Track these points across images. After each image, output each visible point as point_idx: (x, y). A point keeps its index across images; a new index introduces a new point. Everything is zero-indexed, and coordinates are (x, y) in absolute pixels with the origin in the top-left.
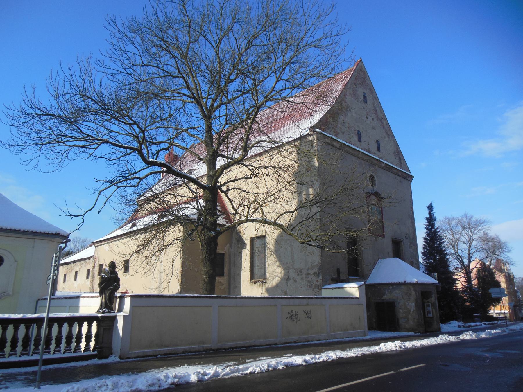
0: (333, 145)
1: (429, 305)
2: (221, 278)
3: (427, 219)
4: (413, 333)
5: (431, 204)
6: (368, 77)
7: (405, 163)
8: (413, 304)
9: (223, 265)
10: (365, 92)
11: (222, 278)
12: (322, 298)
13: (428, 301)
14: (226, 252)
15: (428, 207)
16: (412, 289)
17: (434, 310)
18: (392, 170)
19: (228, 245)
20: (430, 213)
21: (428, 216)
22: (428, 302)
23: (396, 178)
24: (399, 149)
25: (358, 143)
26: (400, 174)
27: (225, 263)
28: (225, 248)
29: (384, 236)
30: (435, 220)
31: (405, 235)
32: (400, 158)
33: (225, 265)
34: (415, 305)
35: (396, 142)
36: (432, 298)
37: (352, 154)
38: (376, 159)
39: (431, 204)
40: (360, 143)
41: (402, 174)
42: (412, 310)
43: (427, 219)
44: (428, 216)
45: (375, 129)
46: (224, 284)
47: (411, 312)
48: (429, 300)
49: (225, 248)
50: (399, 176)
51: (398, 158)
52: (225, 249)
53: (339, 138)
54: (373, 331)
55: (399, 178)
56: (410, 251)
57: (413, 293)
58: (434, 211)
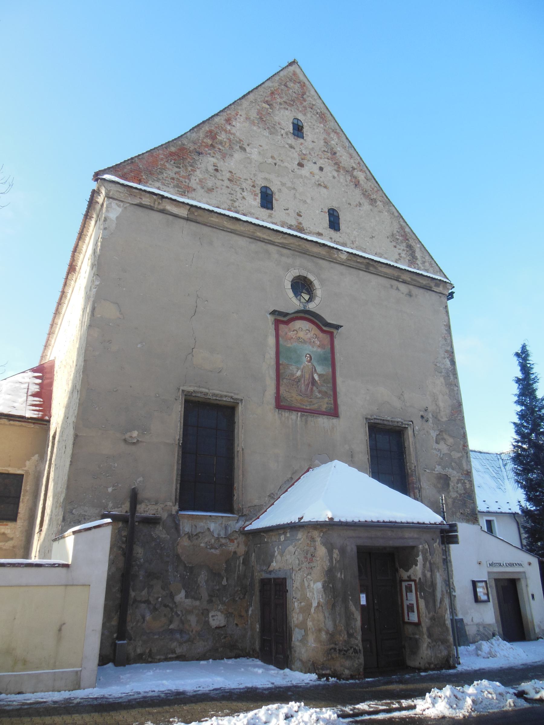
0: (163, 211)
1: (411, 585)
2: (7, 525)
3: (518, 381)
4: (310, 678)
5: (524, 347)
6: (313, 92)
7: (427, 258)
8: (319, 585)
9: (19, 497)
10: (300, 117)
11: (11, 525)
12: (53, 565)
13: (408, 574)
14: (27, 472)
15: (517, 355)
16: (318, 539)
17: (422, 603)
18: (376, 268)
19: (36, 457)
20: (525, 369)
21: (520, 375)
22: (410, 579)
23: (392, 286)
24: (407, 230)
25: (265, 212)
26: (406, 277)
27: (22, 493)
28: (28, 463)
29: (334, 413)
30: (535, 381)
31: (422, 413)
32: (410, 247)
33: (22, 497)
34: (325, 587)
35: (396, 214)
36: (416, 565)
37: (233, 232)
38: (232, 217)
39: (524, 347)
40: (269, 211)
41: (412, 279)
42: (315, 604)
43: (518, 381)
44: (520, 375)
45: (325, 187)
46: (12, 539)
47: (313, 610)
48: (411, 572)
49: (28, 463)
50: (402, 282)
51: (403, 246)
52: (25, 466)
53: (146, 183)
54: (230, 662)
55: (403, 288)
56: (439, 450)
57: (322, 551)
58: (532, 359)
